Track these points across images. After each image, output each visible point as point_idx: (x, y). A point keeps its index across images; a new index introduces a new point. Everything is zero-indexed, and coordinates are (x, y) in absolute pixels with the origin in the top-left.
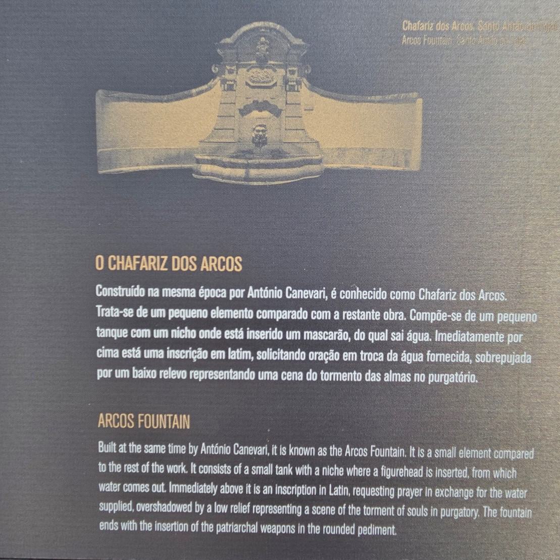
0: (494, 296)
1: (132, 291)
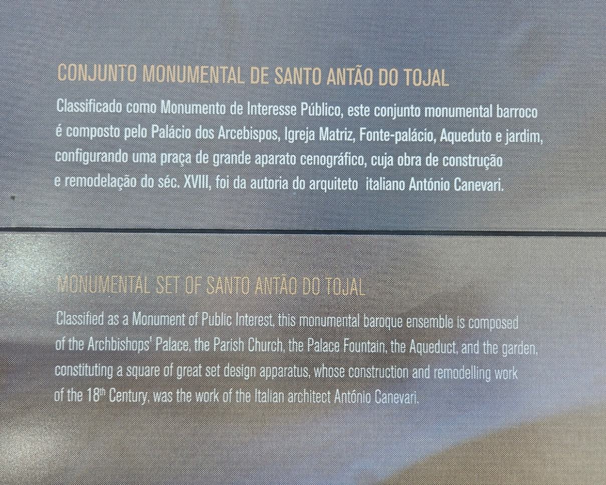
0: (132, 108)
1: (323, 112)
